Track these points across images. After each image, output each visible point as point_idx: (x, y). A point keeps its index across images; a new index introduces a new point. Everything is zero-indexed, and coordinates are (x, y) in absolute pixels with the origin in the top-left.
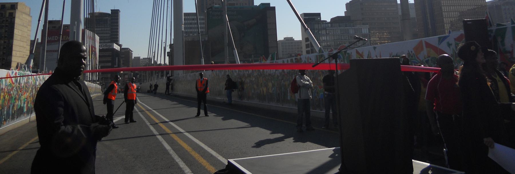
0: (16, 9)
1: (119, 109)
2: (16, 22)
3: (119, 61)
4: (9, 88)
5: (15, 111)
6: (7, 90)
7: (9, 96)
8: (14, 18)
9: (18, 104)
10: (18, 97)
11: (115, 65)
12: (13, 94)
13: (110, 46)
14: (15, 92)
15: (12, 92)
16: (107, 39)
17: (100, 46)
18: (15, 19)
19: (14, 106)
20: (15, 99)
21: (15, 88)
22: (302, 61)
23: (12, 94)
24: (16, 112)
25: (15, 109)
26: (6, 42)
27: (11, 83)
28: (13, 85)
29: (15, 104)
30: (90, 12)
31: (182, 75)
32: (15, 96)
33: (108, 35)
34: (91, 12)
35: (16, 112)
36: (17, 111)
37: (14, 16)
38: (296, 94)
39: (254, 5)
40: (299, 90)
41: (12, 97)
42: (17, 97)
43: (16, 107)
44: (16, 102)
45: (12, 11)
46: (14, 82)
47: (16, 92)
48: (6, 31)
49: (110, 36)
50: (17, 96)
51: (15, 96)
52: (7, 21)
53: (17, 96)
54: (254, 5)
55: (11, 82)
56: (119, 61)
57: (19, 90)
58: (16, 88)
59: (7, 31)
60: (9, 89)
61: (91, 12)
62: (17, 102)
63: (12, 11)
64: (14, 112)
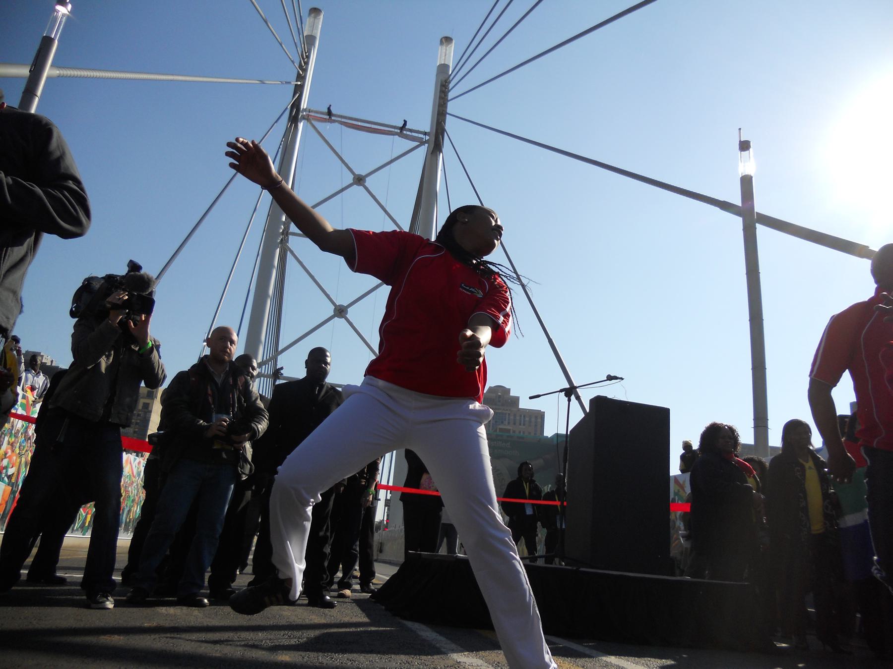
0: (155, 399)
1: (295, 20)
2: (151, 419)
4: (126, 481)
5: (130, 520)
6: (124, 483)
7: (125, 493)
8: (151, 412)
9: (136, 511)
10: (138, 500)
12: (132, 492)
14: (135, 490)
15: (130, 488)
18: (151, 415)
19: (129, 511)
20: (133, 501)
21: (135, 484)
23: (129, 491)
24: (132, 521)
25: (131, 517)
26: (140, 414)
27: (131, 474)
28: (134, 479)
29: (132, 509)
30: (267, 379)
31: (400, 527)
32: (134, 496)
34: (269, 373)
35: (132, 521)
36: (133, 521)
37: (150, 409)
38: (464, 198)
39: (511, 395)
40: (491, 266)
41: (130, 496)
42: (137, 500)
43: (133, 515)
44: (134, 507)
45: (147, 401)
46: (135, 474)
47: (136, 491)
48: (135, 432)
50: (136, 497)
51: (134, 496)
52: (139, 415)
53: (136, 497)
54: (511, 395)
55: (131, 473)
57: (140, 490)
58: (137, 485)
59: (138, 423)
60: (127, 482)
61: (269, 373)
62: (136, 507)
63: (147, 401)
64: (130, 521)
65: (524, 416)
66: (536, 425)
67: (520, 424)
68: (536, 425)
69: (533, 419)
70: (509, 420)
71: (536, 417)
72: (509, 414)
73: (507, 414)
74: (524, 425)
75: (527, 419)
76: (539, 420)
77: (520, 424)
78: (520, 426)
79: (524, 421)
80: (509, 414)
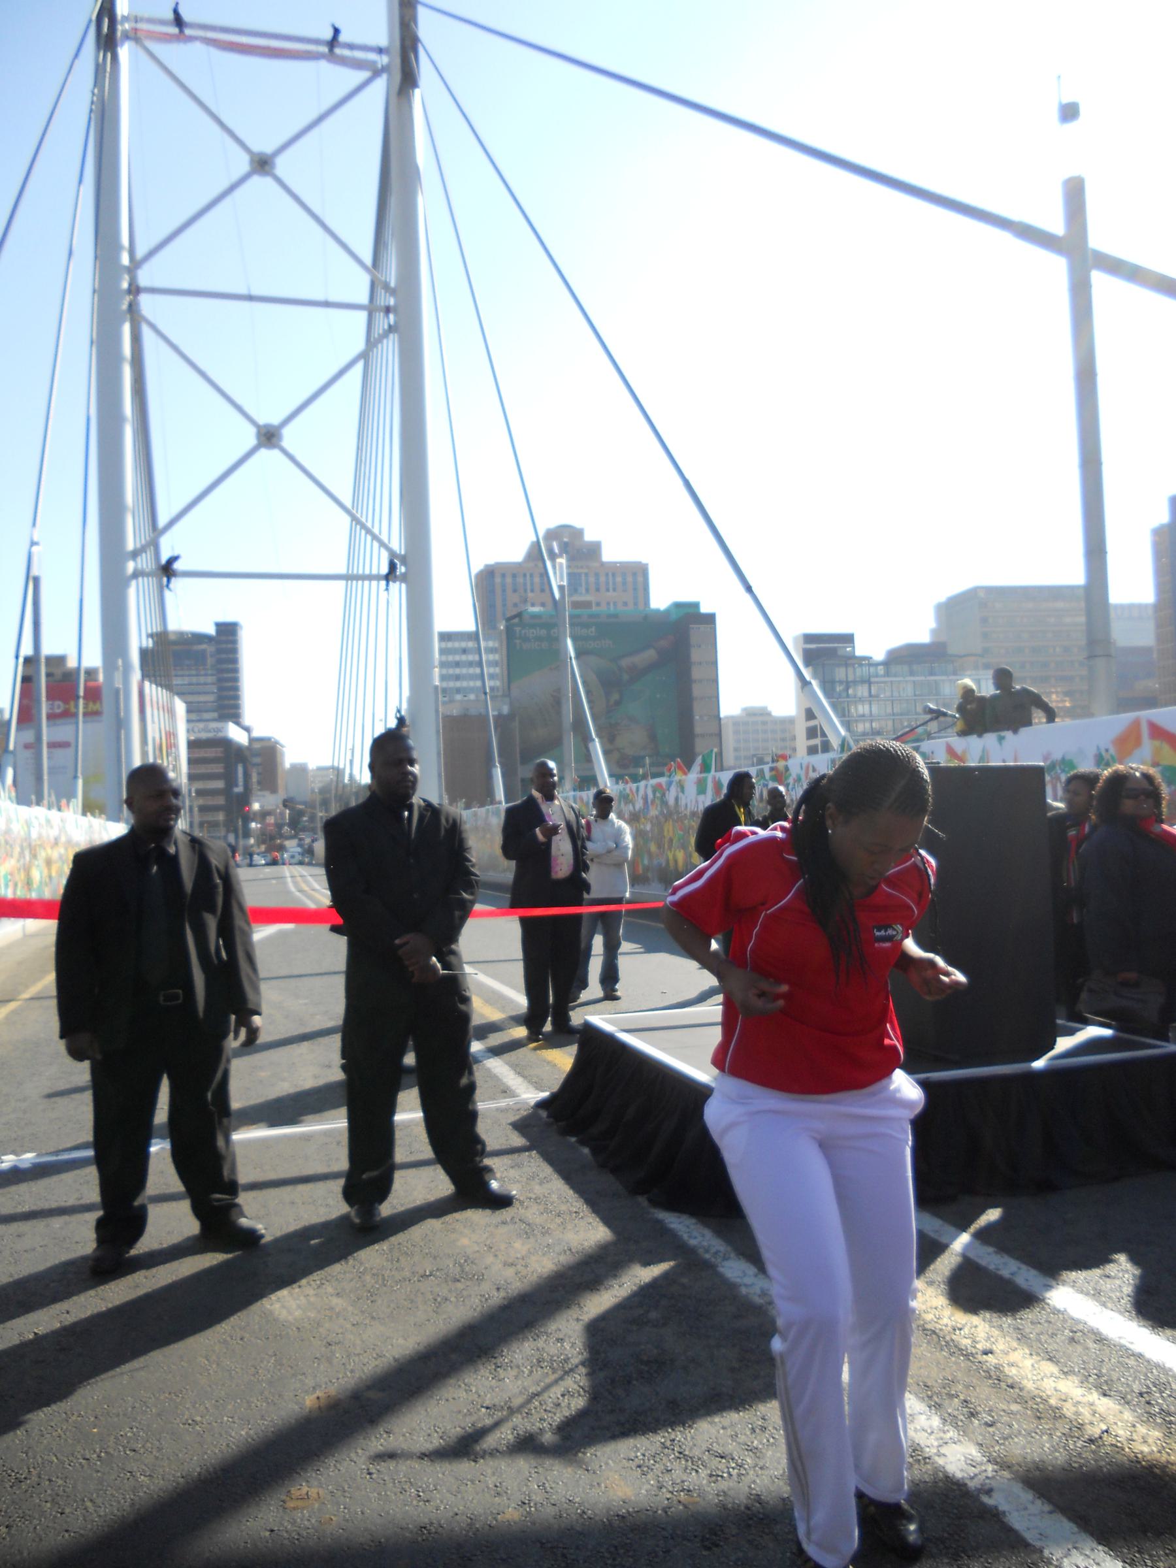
3: (247, 776)
11: (237, 786)
13: (219, 730)
16: (206, 711)
17: (188, 731)
22: (790, 775)
33: (211, 698)
49: (213, 702)
56: (247, 776)
65: (531, 576)
66: (635, 589)
67: (608, 590)
68: (635, 589)
69: (630, 579)
70: (587, 583)
71: (634, 574)
72: (586, 575)
73: (583, 575)
74: (614, 590)
75: (619, 579)
76: (640, 579)
77: (608, 590)
78: (608, 594)
79: (614, 583)
80: (586, 575)
